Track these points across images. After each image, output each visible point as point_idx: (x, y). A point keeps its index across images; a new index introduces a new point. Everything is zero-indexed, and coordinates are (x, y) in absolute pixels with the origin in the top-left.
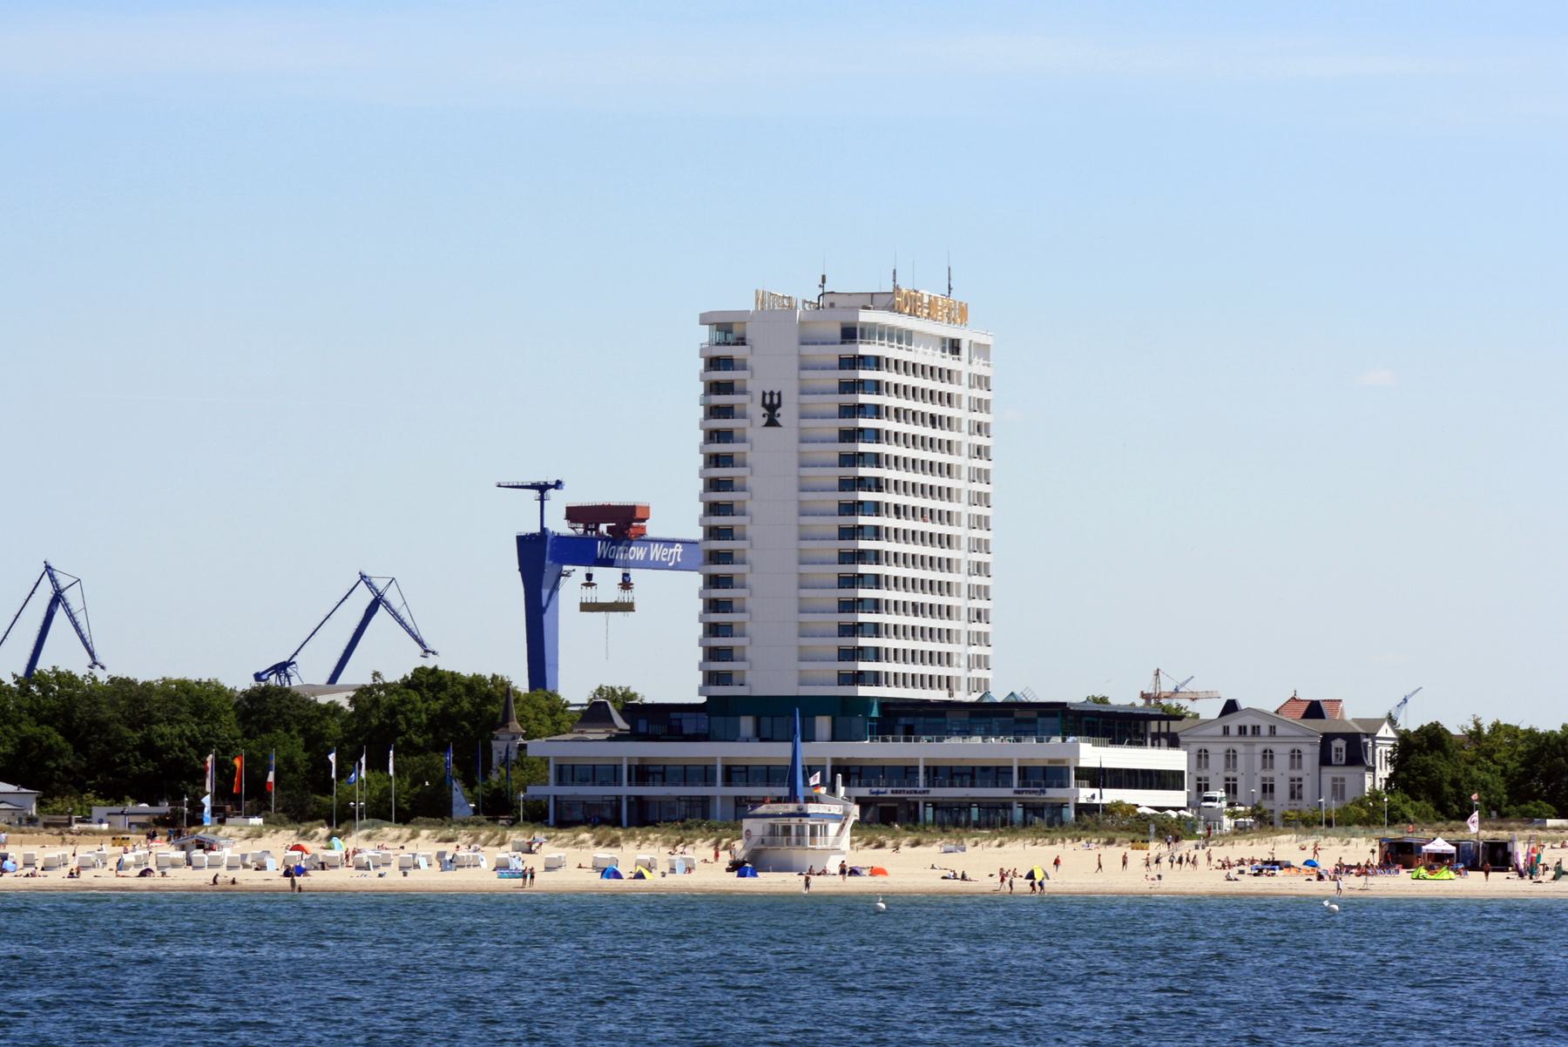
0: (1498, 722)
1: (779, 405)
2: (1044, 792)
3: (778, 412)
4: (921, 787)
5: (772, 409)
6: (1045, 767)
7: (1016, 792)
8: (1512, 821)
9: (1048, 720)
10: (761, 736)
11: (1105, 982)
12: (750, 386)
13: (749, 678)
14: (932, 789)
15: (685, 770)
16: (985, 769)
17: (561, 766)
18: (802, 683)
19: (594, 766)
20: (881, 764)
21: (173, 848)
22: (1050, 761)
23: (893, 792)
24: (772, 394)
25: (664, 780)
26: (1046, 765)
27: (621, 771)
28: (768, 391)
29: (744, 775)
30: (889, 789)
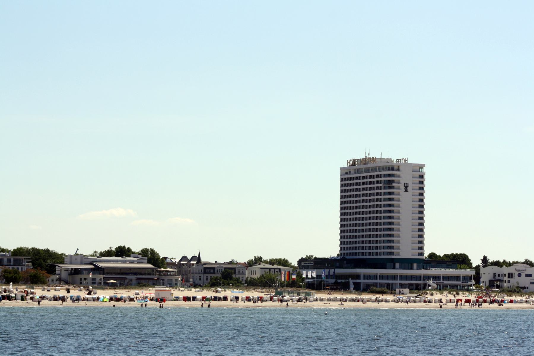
1: (408, 186)
2: (468, 283)
3: (408, 188)
5: (406, 187)
6: (465, 277)
9: (444, 265)
11: (520, 336)
12: (401, 182)
14: (445, 282)
15: (387, 276)
16: (451, 277)
17: (364, 275)
18: (412, 255)
20: (428, 275)
21: (326, 295)
22: (466, 275)
23: (436, 282)
25: (382, 279)
26: (465, 276)
27: (361, 276)
28: (405, 183)
29: (415, 278)
30: (436, 282)
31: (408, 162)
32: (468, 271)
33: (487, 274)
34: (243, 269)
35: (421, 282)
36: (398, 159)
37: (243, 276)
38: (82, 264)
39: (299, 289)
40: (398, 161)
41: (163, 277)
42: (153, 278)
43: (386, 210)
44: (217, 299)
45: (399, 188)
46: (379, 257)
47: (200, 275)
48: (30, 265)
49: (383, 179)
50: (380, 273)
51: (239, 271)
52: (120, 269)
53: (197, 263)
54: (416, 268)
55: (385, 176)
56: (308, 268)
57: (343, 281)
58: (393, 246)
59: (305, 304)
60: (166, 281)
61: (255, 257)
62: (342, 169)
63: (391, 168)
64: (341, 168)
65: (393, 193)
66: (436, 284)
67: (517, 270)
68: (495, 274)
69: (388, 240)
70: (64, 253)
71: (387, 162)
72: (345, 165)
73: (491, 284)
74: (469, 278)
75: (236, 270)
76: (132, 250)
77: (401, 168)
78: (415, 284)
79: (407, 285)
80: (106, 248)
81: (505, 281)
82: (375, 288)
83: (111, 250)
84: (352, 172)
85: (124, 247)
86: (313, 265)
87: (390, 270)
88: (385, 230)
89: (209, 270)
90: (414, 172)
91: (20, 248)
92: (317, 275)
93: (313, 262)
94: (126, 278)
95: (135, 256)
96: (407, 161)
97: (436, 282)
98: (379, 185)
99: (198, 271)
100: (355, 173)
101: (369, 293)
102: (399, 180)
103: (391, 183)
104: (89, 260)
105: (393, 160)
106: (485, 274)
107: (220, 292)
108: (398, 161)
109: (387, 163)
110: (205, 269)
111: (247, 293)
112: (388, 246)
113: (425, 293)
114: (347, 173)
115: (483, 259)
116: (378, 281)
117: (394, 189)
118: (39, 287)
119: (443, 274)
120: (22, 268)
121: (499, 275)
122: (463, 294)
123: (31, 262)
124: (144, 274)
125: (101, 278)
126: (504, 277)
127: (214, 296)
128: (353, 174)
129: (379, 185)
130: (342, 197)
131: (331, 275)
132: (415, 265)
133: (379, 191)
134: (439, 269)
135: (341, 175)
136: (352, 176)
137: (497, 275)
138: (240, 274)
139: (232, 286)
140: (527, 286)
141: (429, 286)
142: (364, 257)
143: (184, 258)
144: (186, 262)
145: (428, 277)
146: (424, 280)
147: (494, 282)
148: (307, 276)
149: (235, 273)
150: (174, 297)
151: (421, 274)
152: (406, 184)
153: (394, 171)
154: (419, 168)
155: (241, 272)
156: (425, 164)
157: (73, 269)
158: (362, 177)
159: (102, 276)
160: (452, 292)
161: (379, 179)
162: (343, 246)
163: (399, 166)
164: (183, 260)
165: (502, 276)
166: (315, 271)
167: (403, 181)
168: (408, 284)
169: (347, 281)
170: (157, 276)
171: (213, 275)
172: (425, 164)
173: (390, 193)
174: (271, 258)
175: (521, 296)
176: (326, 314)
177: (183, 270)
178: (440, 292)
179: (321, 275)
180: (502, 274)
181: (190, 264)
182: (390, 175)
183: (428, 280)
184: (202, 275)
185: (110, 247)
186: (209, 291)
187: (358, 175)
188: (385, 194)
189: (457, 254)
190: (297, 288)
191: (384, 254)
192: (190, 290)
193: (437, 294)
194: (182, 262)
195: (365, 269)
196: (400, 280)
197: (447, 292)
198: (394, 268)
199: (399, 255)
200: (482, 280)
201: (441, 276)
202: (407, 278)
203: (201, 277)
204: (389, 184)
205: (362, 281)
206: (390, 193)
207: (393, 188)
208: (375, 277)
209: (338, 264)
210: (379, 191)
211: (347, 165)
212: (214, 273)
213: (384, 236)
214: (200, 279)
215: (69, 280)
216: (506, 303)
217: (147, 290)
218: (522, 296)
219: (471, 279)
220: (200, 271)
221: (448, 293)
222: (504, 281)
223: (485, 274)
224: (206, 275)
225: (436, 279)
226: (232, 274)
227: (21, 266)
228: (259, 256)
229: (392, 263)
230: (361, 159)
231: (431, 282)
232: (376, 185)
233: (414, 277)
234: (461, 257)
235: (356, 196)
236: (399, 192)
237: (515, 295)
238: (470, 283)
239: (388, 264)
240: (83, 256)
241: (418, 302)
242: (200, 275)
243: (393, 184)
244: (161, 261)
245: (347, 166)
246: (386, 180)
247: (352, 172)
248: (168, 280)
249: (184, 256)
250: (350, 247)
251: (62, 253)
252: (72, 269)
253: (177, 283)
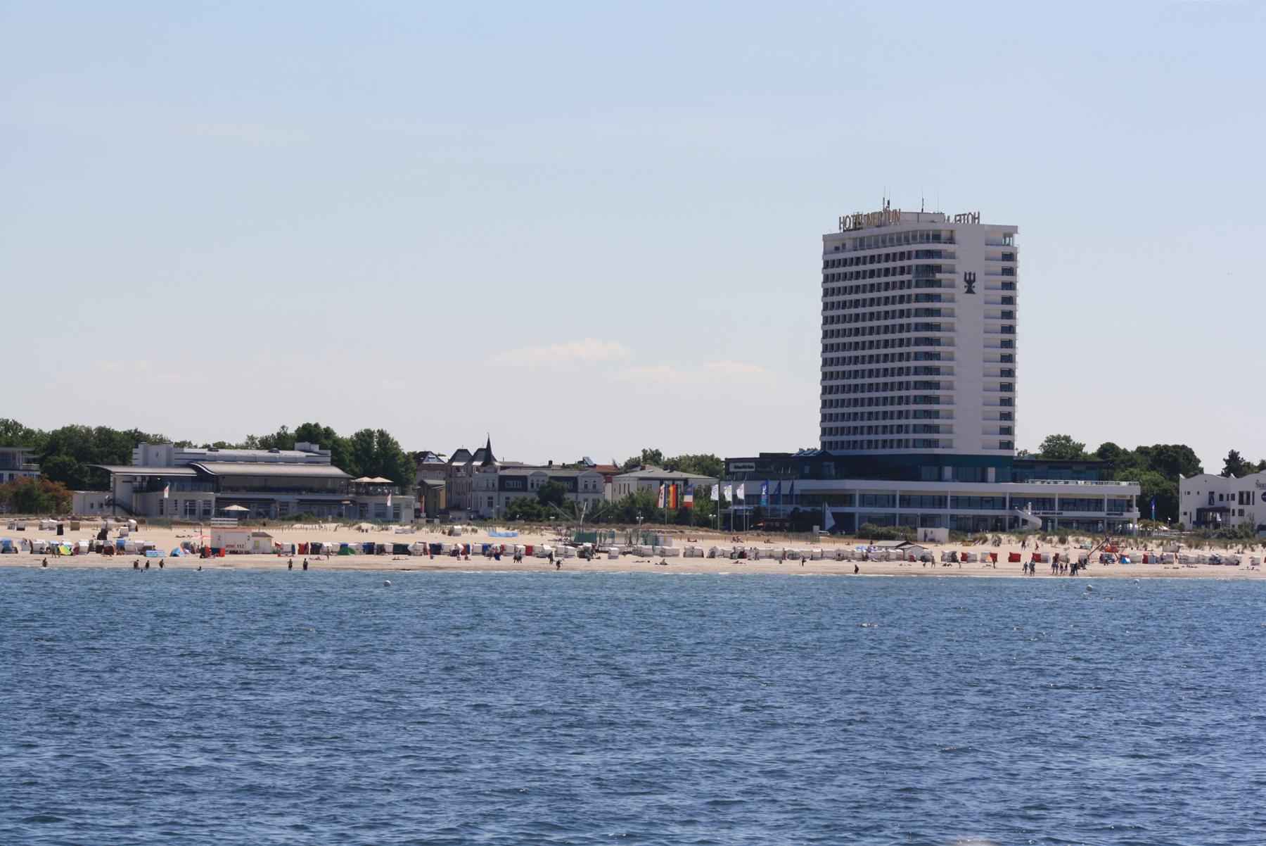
1: (974, 281)
3: (974, 284)
4: (1057, 511)
5: (970, 282)
6: (1115, 500)
8: (615, 527)
12: (957, 268)
13: (955, 443)
16: (1082, 500)
17: (864, 495)
18: (984, 448)
20: (1023, 496)
22: (1118, 496)
24: (970, 274)
25: (993, 506)
28: (968, 272)
30: (1041, 512)
31: (981, 223)
32: (1124, 487)
33: (1193, 493)
34: (596, 479)
35: (1005, 513)
36: (960, 215)
37: (596, 496)
38: (169, 465)
39: (681, 527)
40: (960, 220)
41: (365, 499)
42: (340, 501)
43: (920, 339)
44: (375, 551)
45: (952, 285)
46: (903, 451)
47: (490, 494)
48: (32, 468)
49: (914, 262)
50: (903, 491)
51: (586, 486)
52: (266, 480)
53: (482, 465)
54: (994, 480)
55: (919, 254)
56: (737, 480)
57: (808, 509)
58: (938, 426)
59: (518, 564)
60: (372, 506)
61: (644, 451)
62: (826, 238)
63: (933, 235)
64: (824, 236)
65: (937, 298)
66: (1041, 518)
67: (1259, 485)
68: (1212, 493)
69: (926, 411)
70: (188, 441)
71: (933, 222)
72: (835, 229)
73: (1202, 518)
74: (1126, 504)
75: (579, 481)
76: (335, 434)
77: (957, 237)
78: (992, 516)
79: (971, 521)
80: (271, 430)
81: (1234, 511)
82: (870, 528)
83: (285, 433)
84: (849, 244)
85: (317, 425)
86: (753, 470)
87: (930, 483)
88: (918, 385)
89: (511, 482)
90: (990, 247)
91: (67, 428)
92: (746, 496)
93: (753, 464)
94: (273, 501)
95: (303, 448)
96: (978, 218)
98: (906, 277)
99: (486, 485)
100: (855, 249)
101: (855, 538)
102: (953, 265)
103: (933, 273)
104: (187, 456)
105: (949, 217)
106: (1189, 493)
107: (458, 535)
108: (960, 220)
109: (933, 224)
110: (503, 479)
111: (528, 536)
112: (925, 426)
113: (980, 539)
114: (837, 249)
115: (1227, 458)
116: (898, 510)
117: (940, 286)
118: (29, 519)
119: (1059, 494)
120: (11, 476)
121: (1221, 497)
122: (1077, 541)
123: (34, 461)
124: (319, 491)
125: (210, 499)
126: (1232, 502)
127: (430, 545)
128: (850, 251)
129: (906, 277)
130: (826, 307)
131: (797, 495)
132: (991, 472)
133: (905, 292)
134: (1052, 482)
135: (825, 253)
136: (848, 255)
137: (1216, 497)
138: (588, 492)
139: (555, 520)
141: (1025, 522)
142: (873, 452)
143: (461, 454)
144: (461, 464)
145: (1019, 502)
146: (1011, 507)
147: (1211, 514)
148: (735, 496)
149: (575, 489)
150: (273, 545)
151: (1005, 493)
152: (970, 274)
153: (939, 242)
154: (1002, 236)
155: (590, 487)
156: (1016, 227)
157: (147, 479)
158: (868, 258)
159: (212, 496)
160: (1048, 538)
161: (906, 263)
162: (828, 425)
163: (952, 231)
164: (457, 458)
165: (1228, 499)
166: (743, 485)
167: (962, 267)
168: (974, 516)
169: (819, 508)
170: (350, 495)
171: (521, 495)
172: (1016, 227)
173: (930, 298)
174: (683, 454)
175: (1226, 547)
176: (387, 585)
177: (458, 481)
178: (1017, 538)
179: (759, 496)
180: (1228, 495)
181: (472, 466)
182: (930, 254)
183: (1021, 509)
184: (495, 495)
185: (283, 427)
186: (432, 532)
187: (861, 253)
188: (918, 298)
189: (1166, 447)
190: (678, 527)
191: (916, 443)
192: (387, 529)
193: (1009, 541)
194: (455, 464)
195: (856, 479)
196: (952, 507)
197: (1037, 536)
198: (940, 479)
199: (951, 447)
200: (1182, 509)
201: (1054, 499)
202: (970, 502)
203: (492, 498)
204: (928, 275)
205: (857, 509)
206: (930, 298)
207: (938, 284)
208: (891, 500)
209: (807, 470)
210: (905, 292)
211: (840, 228)
212: (525, 489)
213: (917, 400)
214: (490, 505)
215: (134, 505)
216: (1127, 563)
217: (289, 529)
218: (1229, 546)
219: (1132, 506)
220: (491, 485)
221: (1039, 539)
223: (1189, 493)
224: (504, 494)
225: (1044, 505)
226: (563, 491)
227: (10, 470)
228: (654, 449)
229: (934, 466)
230: (868, 215)
231: (1028, 513)
232: (898, 278)
233: (988, 502)
234: (1176, 452)
235: (856, 303)
236: (953, 295)
237: (1209, 545)
238: (1126, 515)
239: (925, 470)
240: (172, 446)
241: (893, 560)
242: (490, 494)
243: (938, 276)
244: (403, 460)
245: (839, 232)
246: (922, 266)
247: (849, 244)
248: (376, 504)
249: (460, 448)
250: (843, 428)
251: (183, 440)
252: (143, 478)
253: (398, 514)
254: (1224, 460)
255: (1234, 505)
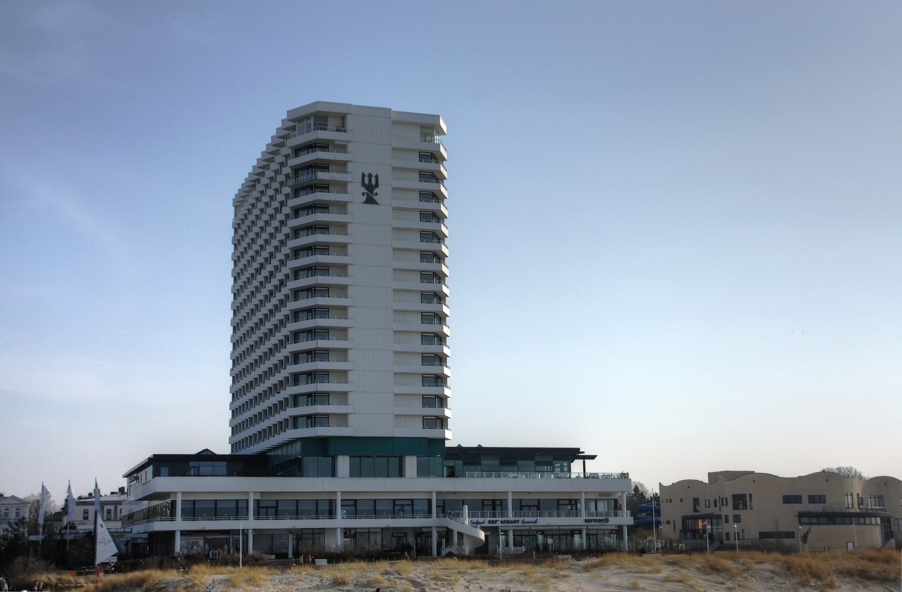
0: (579, 449)
1: (377, 185)
5: (370, 187)
7: (587, 521)
10: (356, 472)
19: (520, 500)
25: (277, 514)
28: (367, 174)
64: (809, 496)
81: (726, 517)
97: (490, 522)
106: (671, 501)
126: (723, 508)
137: (702, 502)
140: (783, 528)
165: (715, 505)
180: (715, 501)
222: (723, 517)
225: (494, 509)
254: (660, 484)
255: (728, 510)
